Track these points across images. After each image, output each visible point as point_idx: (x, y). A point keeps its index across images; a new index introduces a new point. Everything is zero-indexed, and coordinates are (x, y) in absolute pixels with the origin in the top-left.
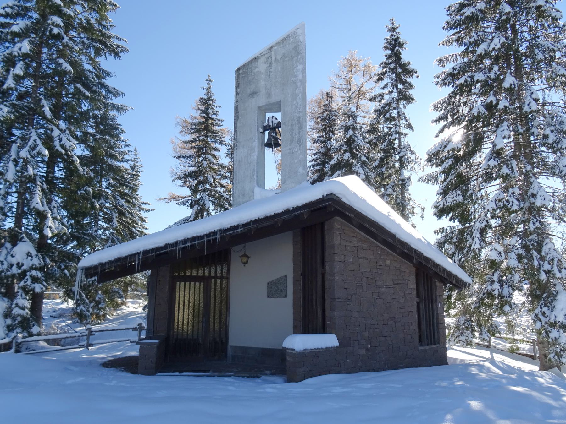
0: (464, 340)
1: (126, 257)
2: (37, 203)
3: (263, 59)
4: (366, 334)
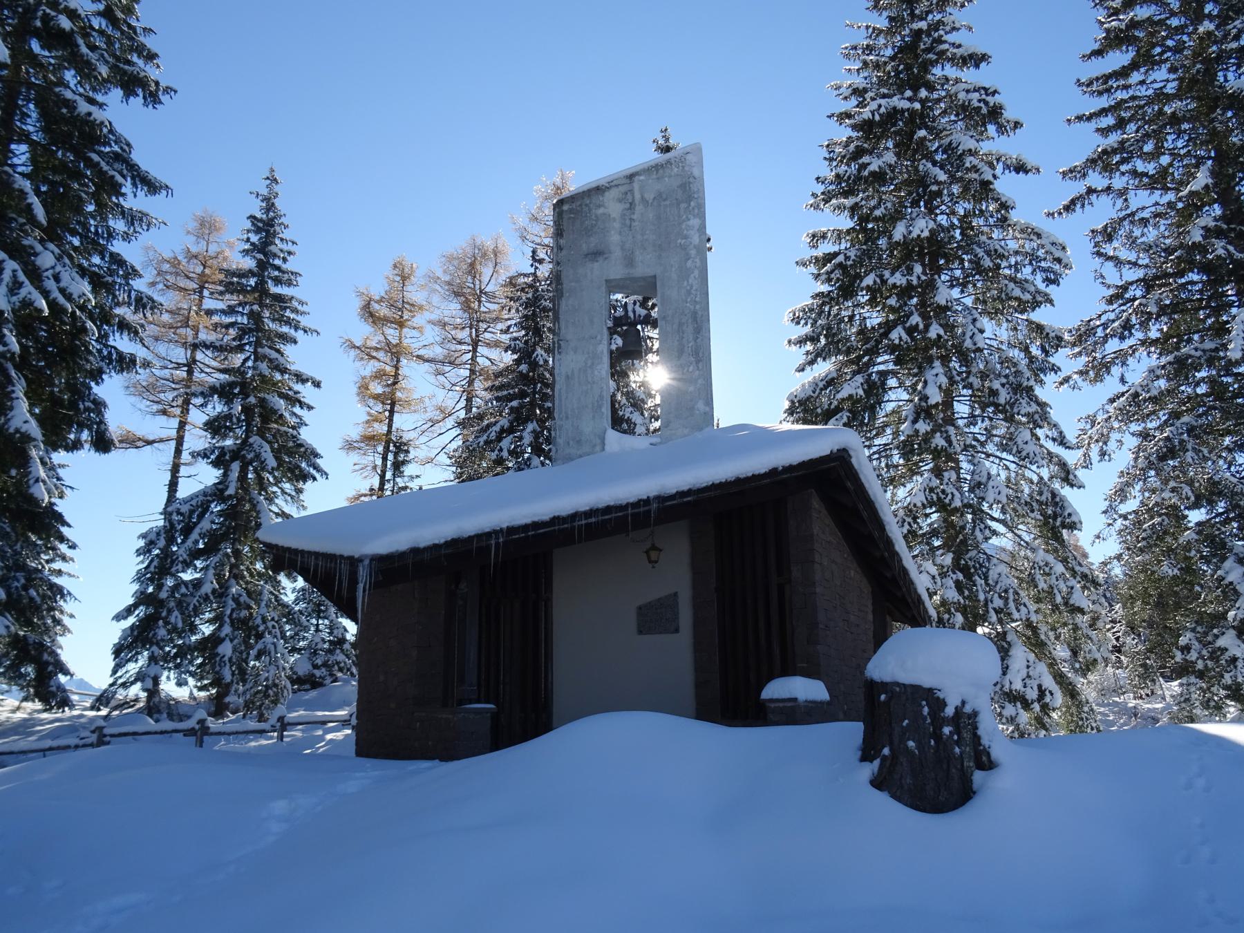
1: (470, 538)
2: (26, 422)
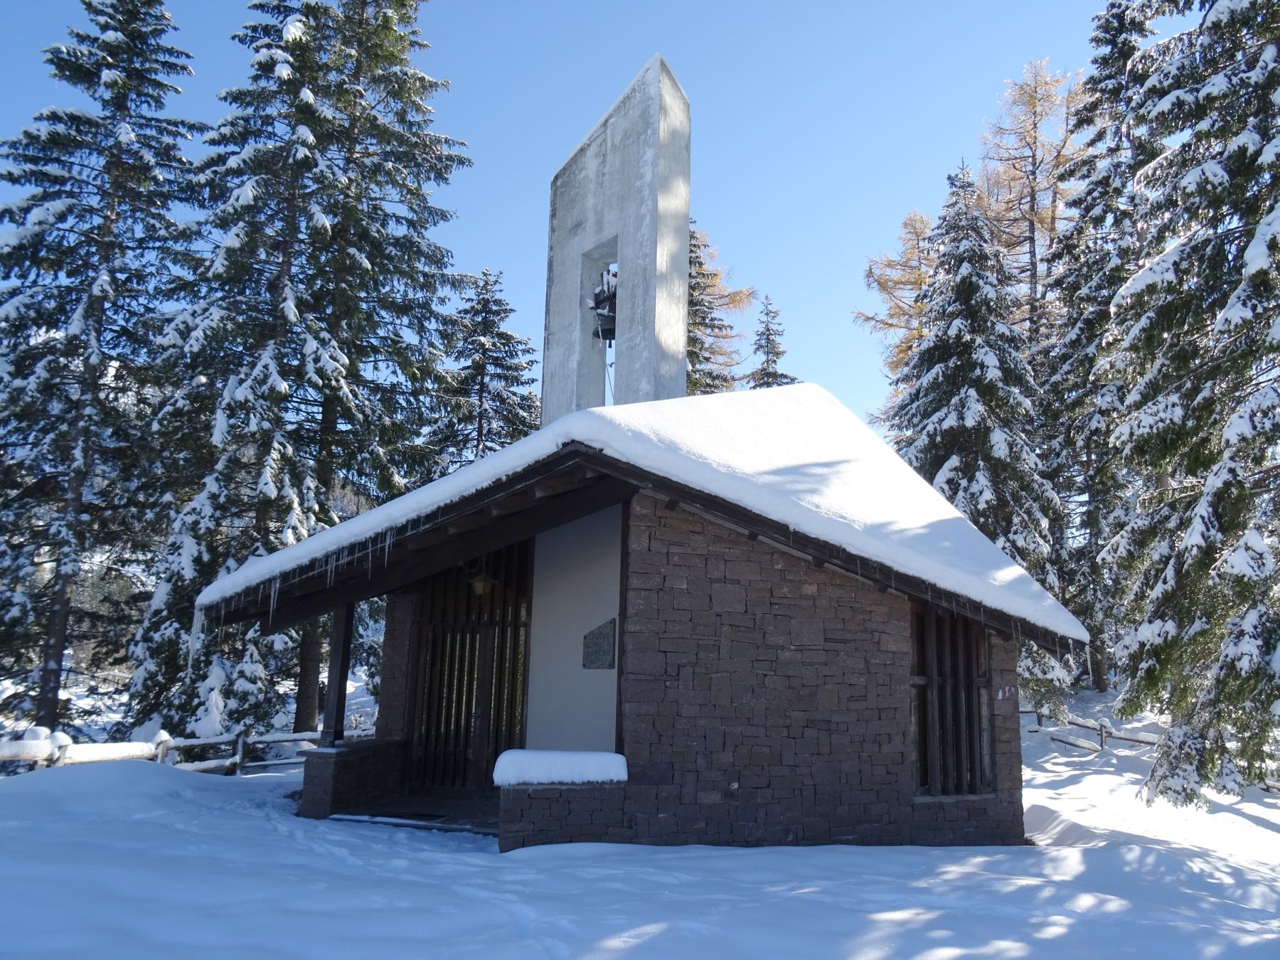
0: (1179, 788)
3: (591, 152)
4: (727, 757)
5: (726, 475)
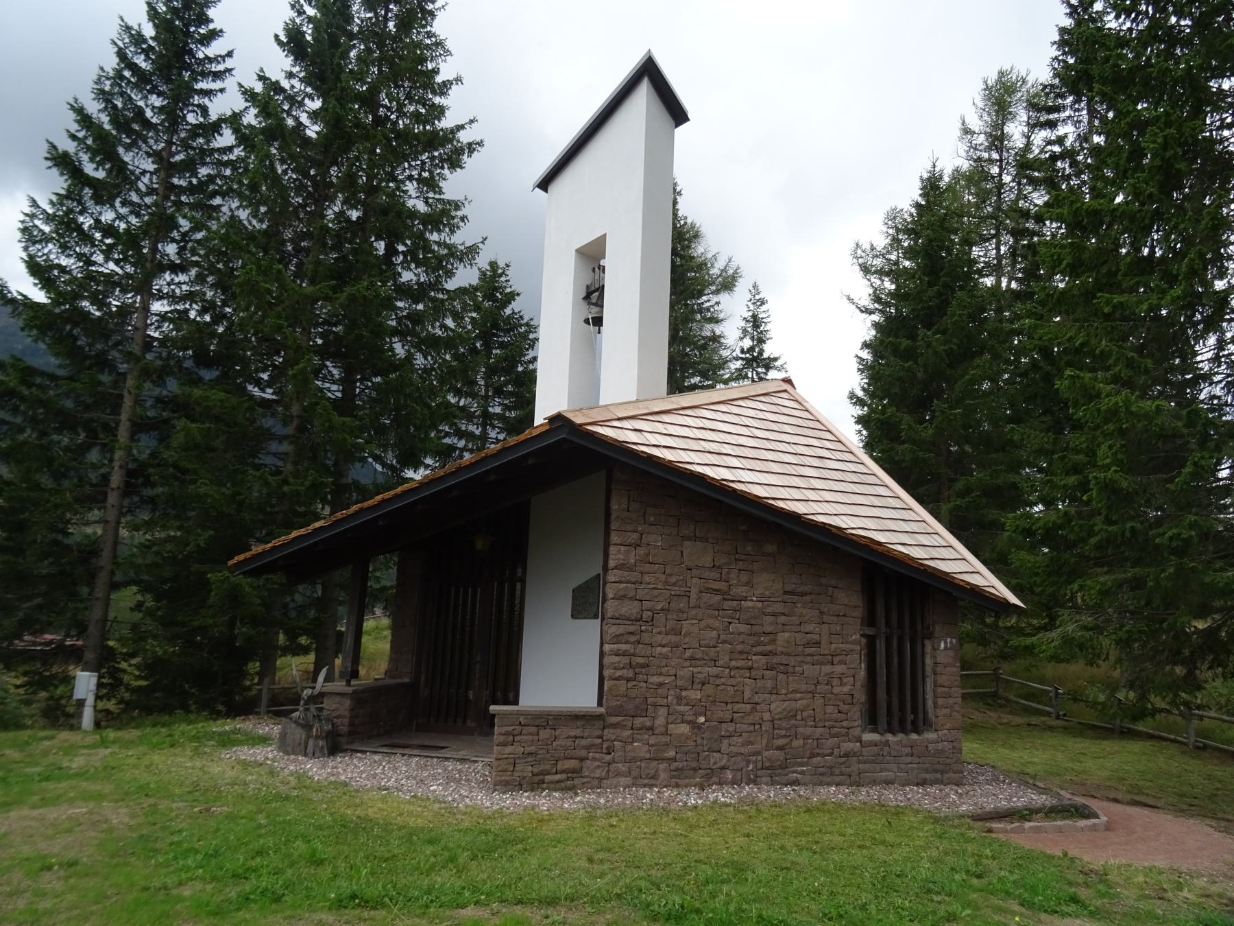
4: (695, 695)
5: (25, 305)
